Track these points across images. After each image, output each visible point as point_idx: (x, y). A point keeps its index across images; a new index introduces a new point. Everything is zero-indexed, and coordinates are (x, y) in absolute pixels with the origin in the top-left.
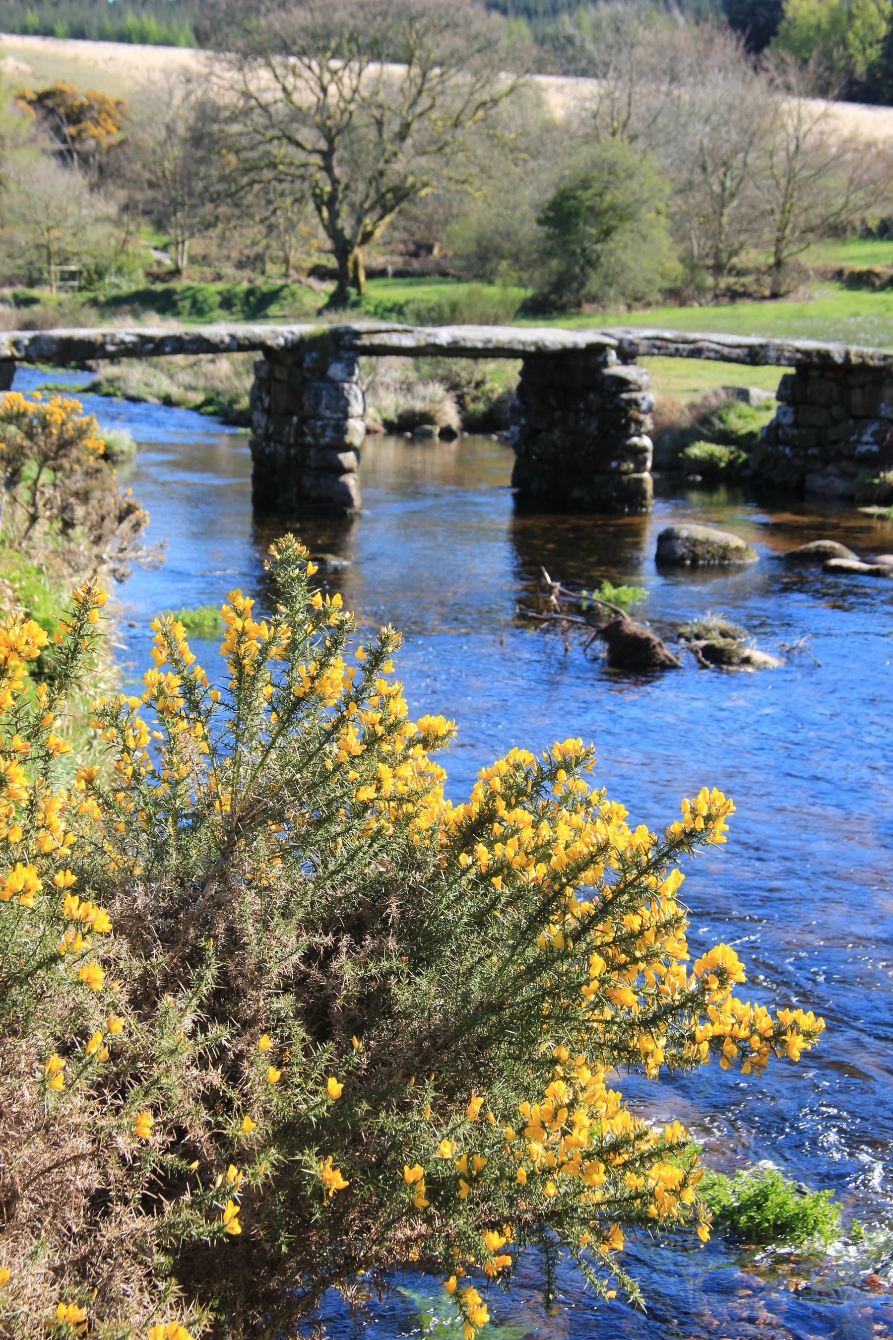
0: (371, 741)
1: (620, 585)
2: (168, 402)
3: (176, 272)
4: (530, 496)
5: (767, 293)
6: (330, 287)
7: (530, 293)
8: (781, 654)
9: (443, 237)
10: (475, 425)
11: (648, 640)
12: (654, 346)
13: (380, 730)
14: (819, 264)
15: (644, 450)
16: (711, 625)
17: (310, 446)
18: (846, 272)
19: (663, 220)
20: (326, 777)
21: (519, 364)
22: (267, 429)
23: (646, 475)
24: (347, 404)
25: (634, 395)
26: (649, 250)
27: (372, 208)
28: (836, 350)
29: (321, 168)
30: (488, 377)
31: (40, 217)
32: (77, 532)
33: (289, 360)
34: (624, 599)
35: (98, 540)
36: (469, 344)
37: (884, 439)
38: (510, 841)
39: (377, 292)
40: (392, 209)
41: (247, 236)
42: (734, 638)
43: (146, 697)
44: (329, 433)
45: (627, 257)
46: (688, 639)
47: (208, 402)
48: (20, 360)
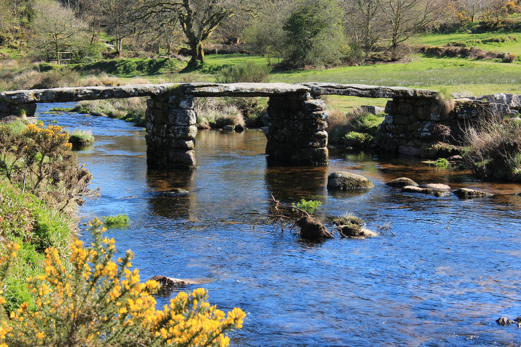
0: (124, 292)
1: (309, 200)
2: (111, 116)
3: (117, 53)
4: (274, 158)
5: (390, 59)
6: (189, 59)
7: (281, 60)
8: (378, 230)
9: (241, 35)
10: (251, 124)
11: (318, 225)
12: (328, 90)
13: (128, 287)
14: (413, 45)
15: (324, 137)
16: (348, 218)
17: (172, 138)
18: (426, 49)
19: (340, 26)
20: (106, 305)
21: (268, 99)
22: (153, 130)
23: (325, 148)
24: (189, 119)
25: (319, 112)
26: (335, 40)
27: (207, 22)
28: (410, 90)
29: (183, 5)
30: (258, 102)
31: (53, 30)
32: (61, 183)
33: (162, 99)
34: (311, 206)
35: (69, 187)
36: (243, 91)
37: (433, 130)
38: (175, 327)
39: (209, 61)
40: (216, 24)
41: (149, 37)
42: (358, 224)
43: (46, 276)
44: (181, 132)
45: (324, 44)
46: (337, 225)
47: (129, 116)
48: (38, 102)
